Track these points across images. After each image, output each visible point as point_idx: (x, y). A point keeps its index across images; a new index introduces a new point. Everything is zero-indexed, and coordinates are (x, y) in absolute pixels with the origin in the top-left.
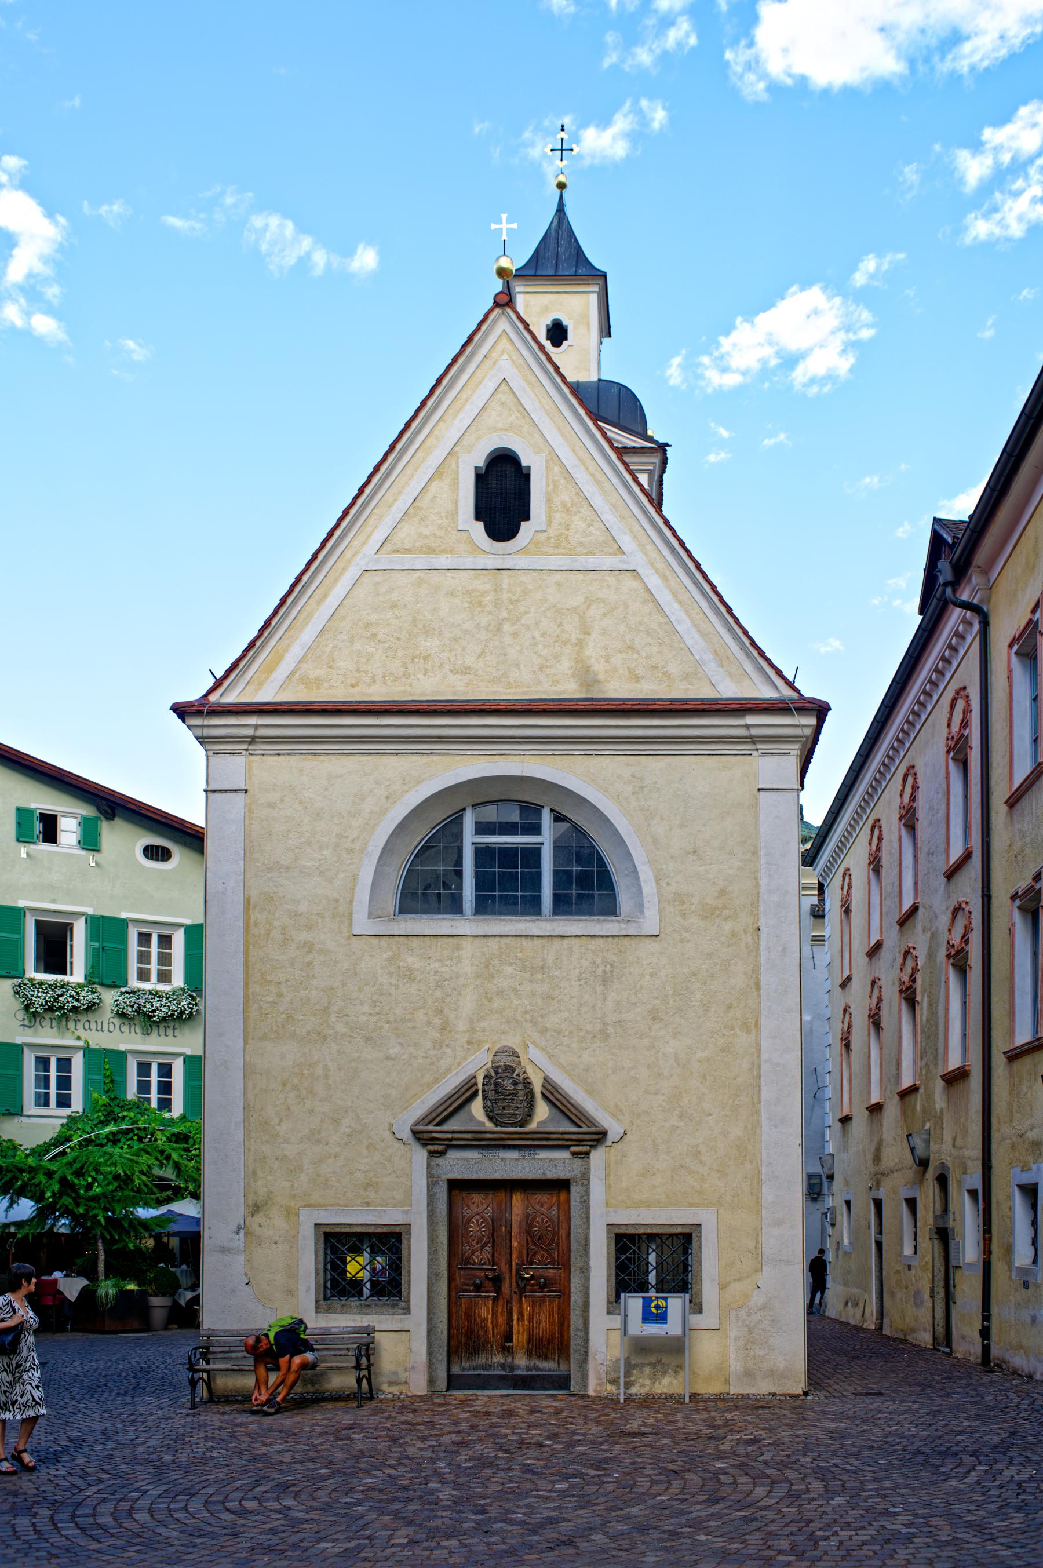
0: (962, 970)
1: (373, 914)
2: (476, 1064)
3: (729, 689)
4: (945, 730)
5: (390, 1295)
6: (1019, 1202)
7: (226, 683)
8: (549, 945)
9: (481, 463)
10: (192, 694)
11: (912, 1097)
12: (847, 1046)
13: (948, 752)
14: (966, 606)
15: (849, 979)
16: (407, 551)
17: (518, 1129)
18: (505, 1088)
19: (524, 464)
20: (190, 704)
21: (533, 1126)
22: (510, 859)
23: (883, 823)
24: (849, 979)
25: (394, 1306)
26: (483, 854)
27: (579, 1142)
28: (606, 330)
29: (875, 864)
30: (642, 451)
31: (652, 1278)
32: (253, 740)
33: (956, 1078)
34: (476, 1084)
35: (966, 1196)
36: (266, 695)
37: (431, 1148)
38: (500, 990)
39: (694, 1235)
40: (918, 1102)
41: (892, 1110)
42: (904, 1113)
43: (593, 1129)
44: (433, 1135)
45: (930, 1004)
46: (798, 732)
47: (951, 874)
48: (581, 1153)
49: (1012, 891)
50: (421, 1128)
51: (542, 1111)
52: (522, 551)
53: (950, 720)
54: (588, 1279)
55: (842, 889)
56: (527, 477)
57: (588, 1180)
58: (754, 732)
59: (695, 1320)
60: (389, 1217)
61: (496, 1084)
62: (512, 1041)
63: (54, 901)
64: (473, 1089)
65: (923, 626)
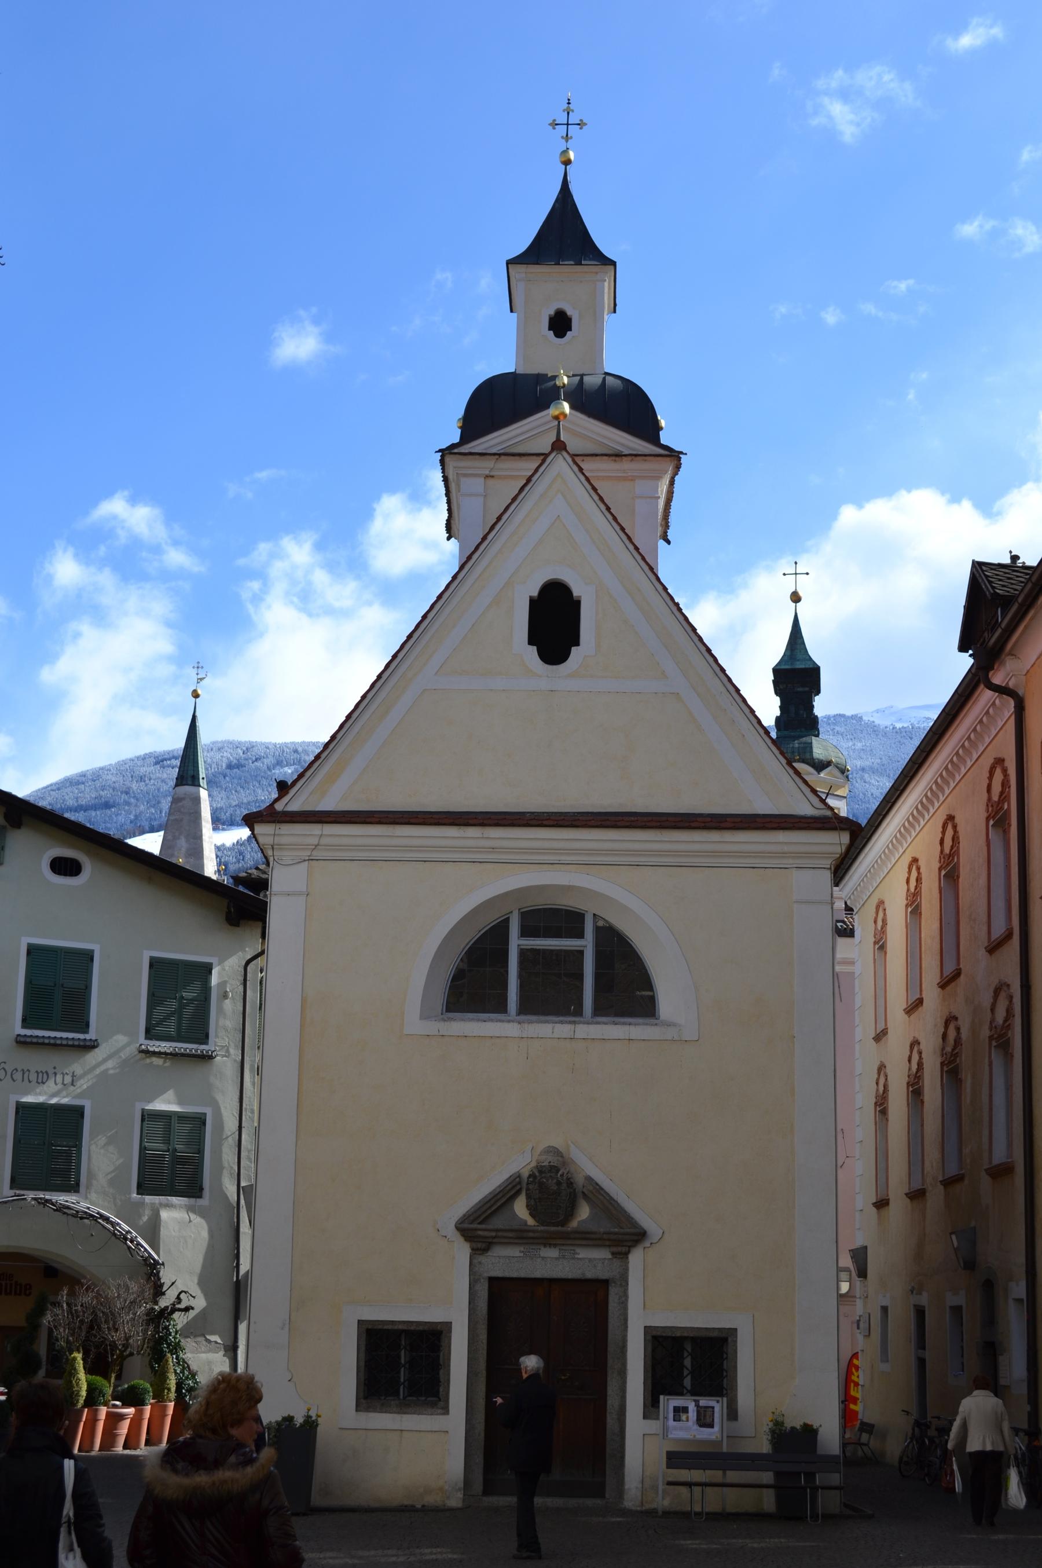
0: (1008, 1056)
1: (424, 1016)
2: (521, 1162)
8: (595, 1040)
12: (884, 1112)
13: (988, 819)
14: (1003, 690)
17: (560, 1228)
18: (553, 1195)
19: (575, 594)
21: (574, 1224)
31: (687, 1382)
33: (1001, 1172)
34: (520, 1183)
36: (328, 804)
37: (615, 1249)
38: (540, 1087)
39: (730, 1339)
41: (936, 1196)
43: (632, 1230)
44: (480, 1228)
48: (620, 1253)
50: (466, 1226)
51: (584, 1212)
55: (875, 922)
56: (578, 603)
60: (432, 1315)
61: (541, 1184)
62: (557, 1142)
64: (518, 1187)
65: (959, 692)
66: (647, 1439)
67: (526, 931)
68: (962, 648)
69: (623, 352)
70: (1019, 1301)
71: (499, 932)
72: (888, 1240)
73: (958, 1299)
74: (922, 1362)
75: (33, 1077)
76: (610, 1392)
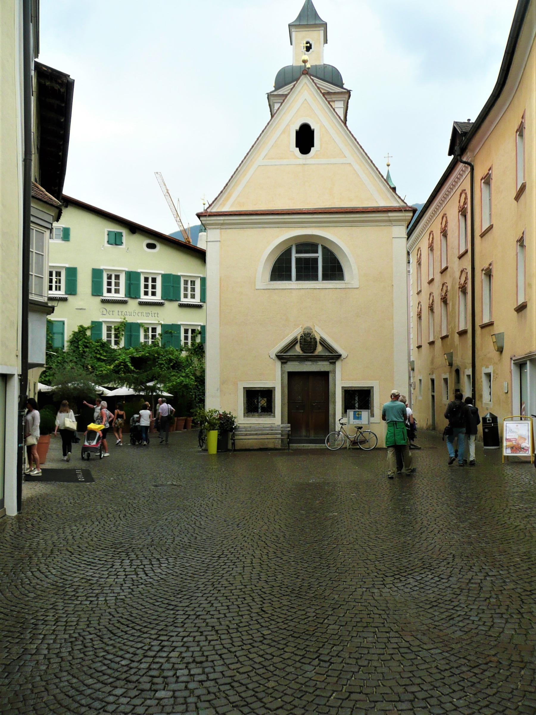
2: (296, 332)
3: (382, 203)
4: (458, 204)
5: (268, 411)
6: (484, 379)
7: (213, 205)
8: (320, 285)
9: (298, 128)
10: (201, 210)
11: (446, 339)
12: (420, 318)
13: (459, 212)
14: (465, 163)
15: (420, 291)
16: (273, 159)
18: (308, 343)
19: (312, 128)
20: (202, 213)
21: (316, 353)
22: (307, 262)
23: (434, 232)
24: (420, 291)
25: (270, 415)
26: (298, 260)
27: (332, 359)
28: (326, 42)
29: (431, 248)
30: (341, 93)
31: (357, 405)
32: (222, 224)
35: (466, 376)
36: (226, 209)
37: (282, 361)
38: (307, 306)
40: (449, 340)
41: (438, 343)
42: (443, 345)
44: (283, 357)
45: (453, 305)
46: (407, 218)
47: (460, 257)
49: (482, 268)
51: (319, 348)
52: (312, 158)
53: (460, 200)
54: (335, 406)
57: (335, 372)
58: (391, 218)
59: (372, 420)
61: (305, 339)
63: (114, 266)
66: (343, 422)
67: (297, 252)
68: (450, 154)
69: (328, 56)
70: (469, 376)
71: (288, 252)
72: (421, 361)
73: (447, 376)
74: (433, 397)
75: (145, 314)
76: (330, 409)
